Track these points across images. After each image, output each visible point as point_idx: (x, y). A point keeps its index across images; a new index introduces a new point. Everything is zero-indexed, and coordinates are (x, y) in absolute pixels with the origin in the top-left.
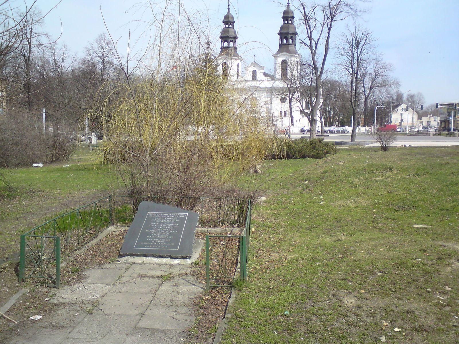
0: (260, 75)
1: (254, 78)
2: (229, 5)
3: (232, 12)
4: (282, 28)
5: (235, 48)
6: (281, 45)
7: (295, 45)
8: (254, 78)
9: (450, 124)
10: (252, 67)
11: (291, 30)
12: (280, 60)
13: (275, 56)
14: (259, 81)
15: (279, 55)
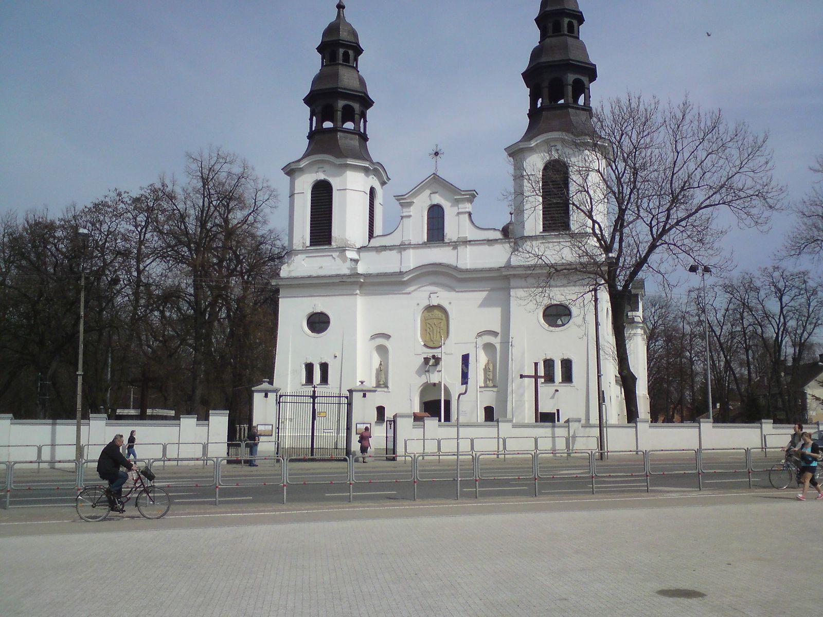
3: (350, 16)
14: (455, 245)
15: (533, 144)
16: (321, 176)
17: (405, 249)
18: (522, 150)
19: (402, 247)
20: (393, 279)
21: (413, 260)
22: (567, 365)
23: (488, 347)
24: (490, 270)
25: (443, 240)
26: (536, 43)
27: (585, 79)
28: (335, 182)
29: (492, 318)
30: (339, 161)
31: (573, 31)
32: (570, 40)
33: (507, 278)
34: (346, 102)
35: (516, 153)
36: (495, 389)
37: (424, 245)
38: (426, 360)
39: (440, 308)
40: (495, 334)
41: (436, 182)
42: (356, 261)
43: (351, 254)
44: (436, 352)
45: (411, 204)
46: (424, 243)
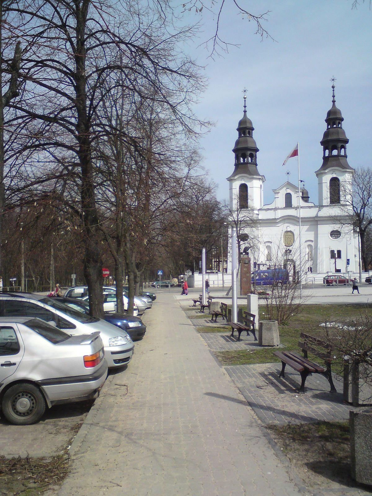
0: (296, 200)
1: (288, 203)
2: (245, 107)
3: (249, 116)
4: (237, 143)
5: (345, 156)
6: (237, 165)
7: (256, 165)
8: (288, 203)
9: (200, 262)
10: (285, 188)
11: (250, 145)
12: (327, 179)
13: (319, 174)
14: (296, 208)
15: (236, 177)
16: (243, 182)
17: (277, 210)
18: (232, 180)
19: (276, 209)
20: (266, 222)
21: (280, 214)
22: (339, 252)
23: (310, 246)
24: (310, 218)
25: (291, 206)
26: (325, 129)
27: (254, 153)
28: (249, 184)
29: (311, 236)
30: (344, 170)
31: (250, 134)
32: (249, 139)
33: (317, 221)
34: (251, 152)
35: (230, 180)
36: (312, 261)
37: (284, 208)
38: (286, 251)
39: (290, 231)
40: (312, 241)
41: (289, 185)
42: (258, 214)
43: (256, 212)
44: (290, 248)
45: (278, 193)
46: (284, 208)
